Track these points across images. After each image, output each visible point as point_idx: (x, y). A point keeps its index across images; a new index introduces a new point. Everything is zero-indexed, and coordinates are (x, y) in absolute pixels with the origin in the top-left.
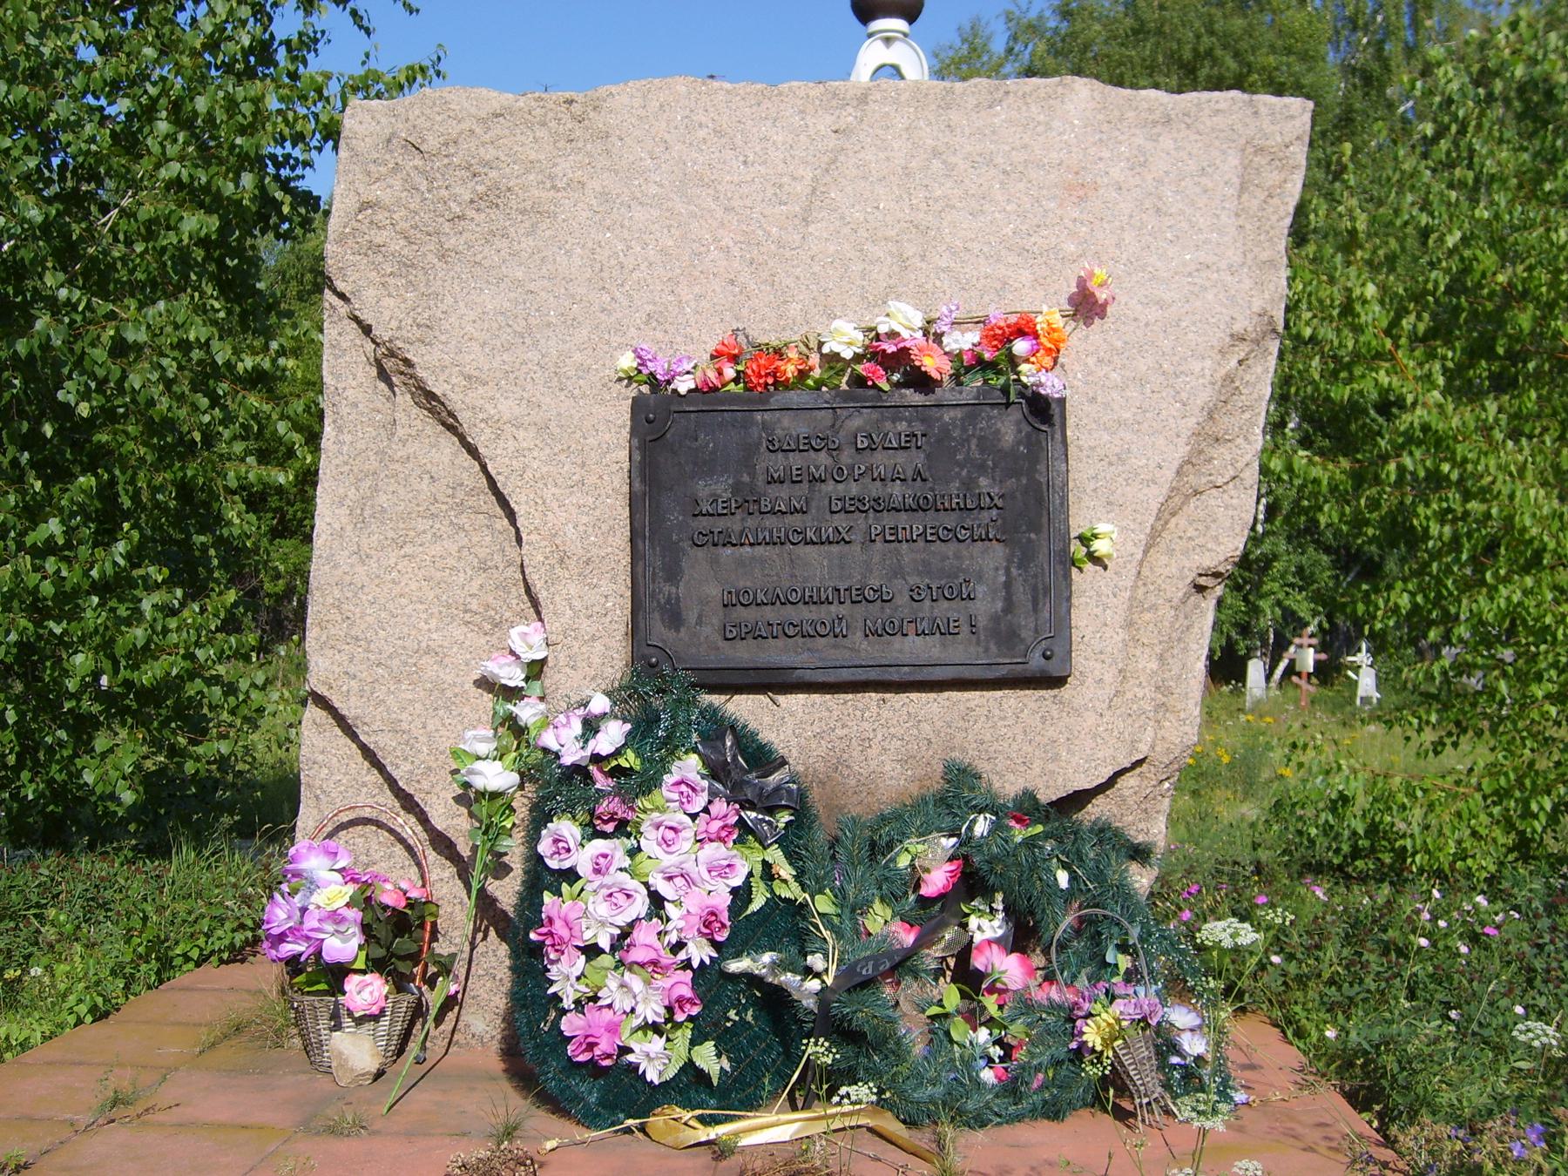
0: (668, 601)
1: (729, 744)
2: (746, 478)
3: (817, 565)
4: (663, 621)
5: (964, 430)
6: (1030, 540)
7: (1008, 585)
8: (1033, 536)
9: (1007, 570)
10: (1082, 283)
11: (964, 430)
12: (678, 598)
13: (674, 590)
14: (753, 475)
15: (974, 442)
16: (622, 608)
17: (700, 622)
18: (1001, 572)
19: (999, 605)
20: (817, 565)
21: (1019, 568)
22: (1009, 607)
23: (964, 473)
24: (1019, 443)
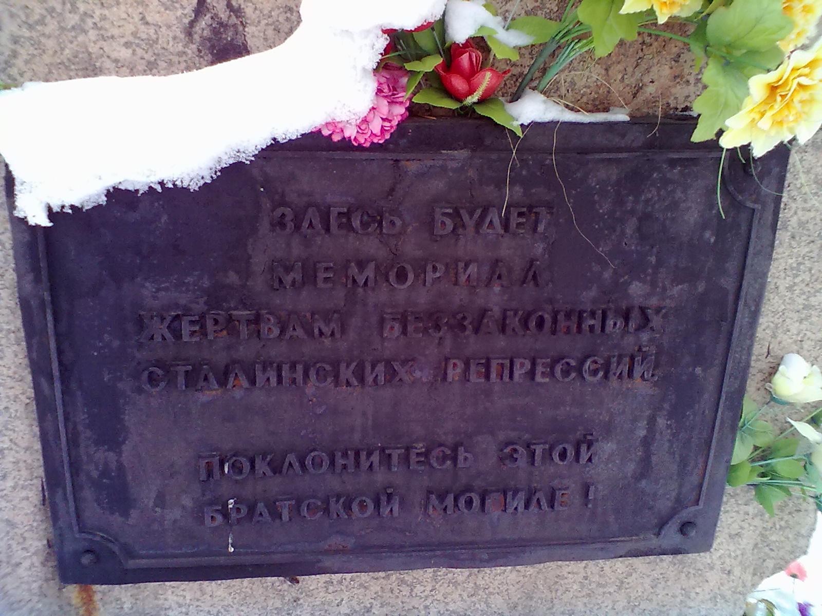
0: (105, 473)
1: (241, 550)
2: (232, 278)
3: (357, 407)
4: (99, 502)
5: (619, 201)
6: (693, 377)
7: (647, 442)
8: (698, 370)
9: (652, 421)
10: (754, 445)
11: (619, 201)
12: (121, 467)
13: (111, 456)
14: (246, 273)
15: (633, 223)
16: (30, 468)
17: (161, 500)
18: (643, 423)
19: (631, 467)
20: (357, 407)
21: (670, 416)
22: (645, 468)
23: (607, 275)
24: (704, 226)
